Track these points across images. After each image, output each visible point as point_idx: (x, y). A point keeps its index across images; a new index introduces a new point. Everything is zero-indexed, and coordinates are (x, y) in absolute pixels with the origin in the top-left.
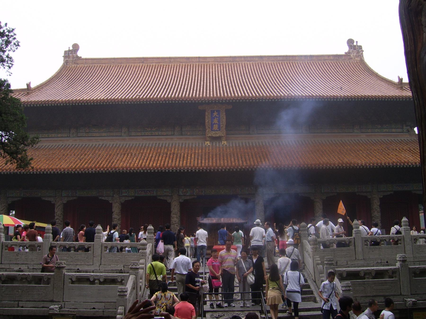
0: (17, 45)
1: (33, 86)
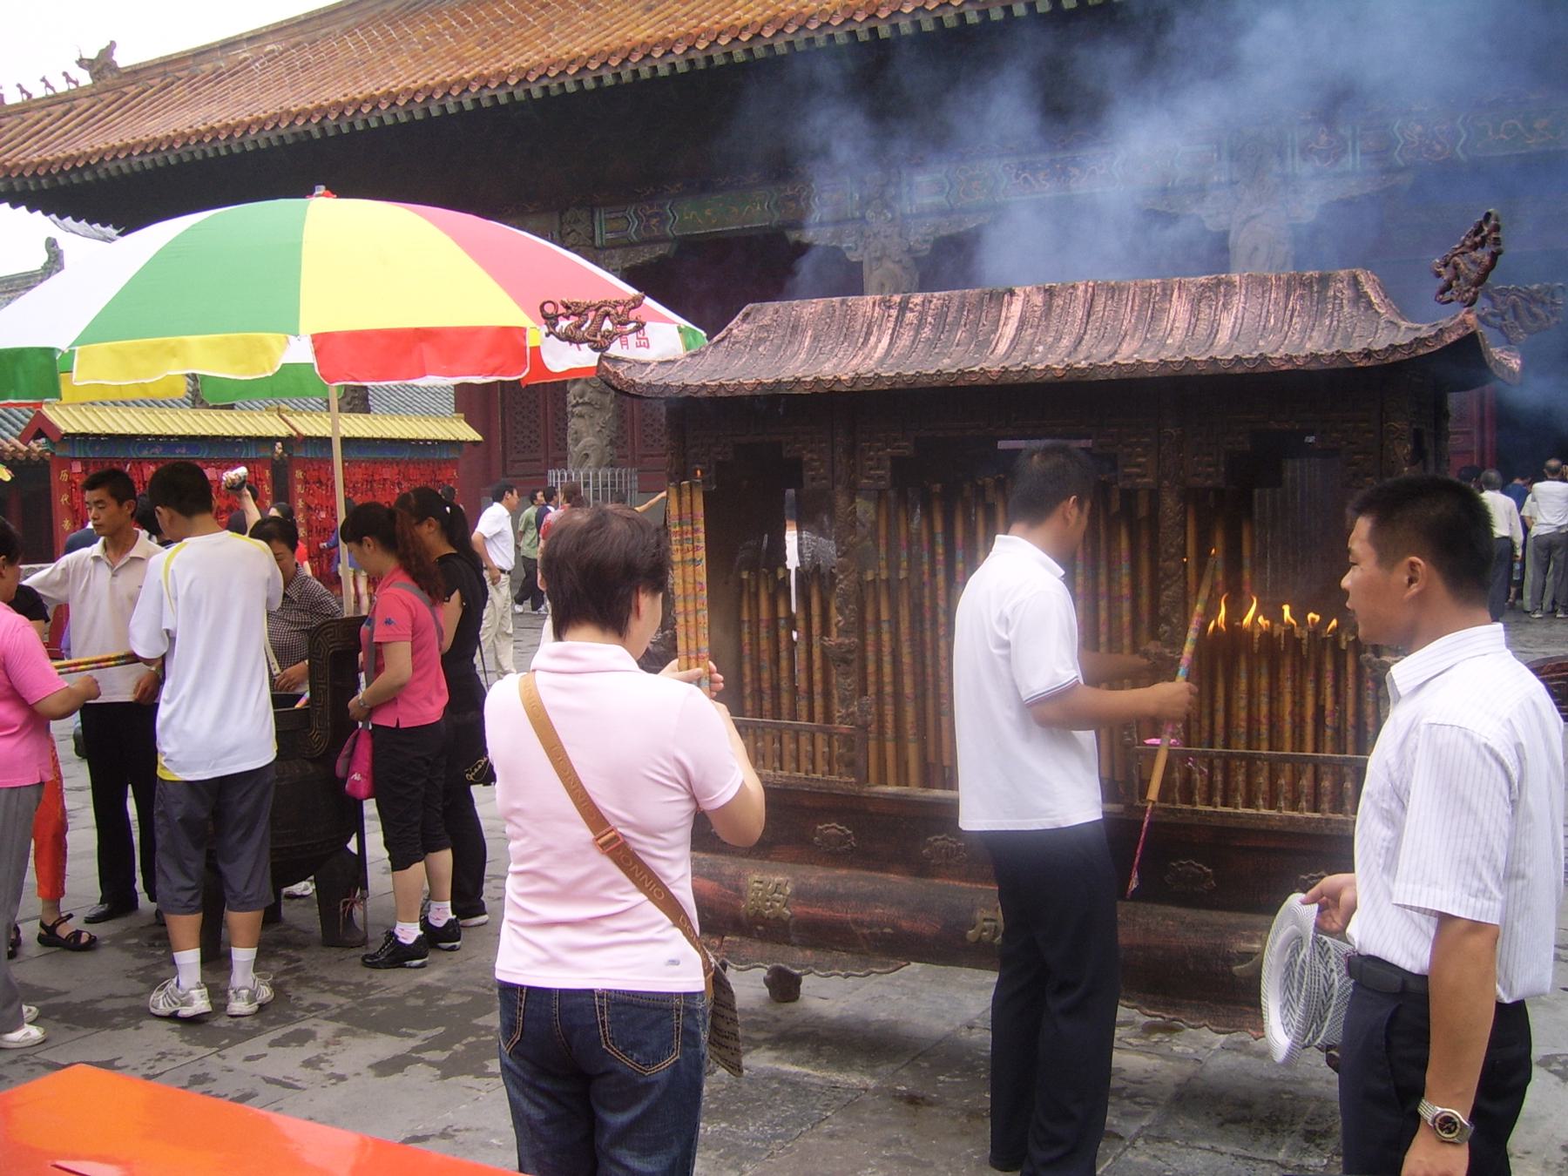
1: (123, 59)
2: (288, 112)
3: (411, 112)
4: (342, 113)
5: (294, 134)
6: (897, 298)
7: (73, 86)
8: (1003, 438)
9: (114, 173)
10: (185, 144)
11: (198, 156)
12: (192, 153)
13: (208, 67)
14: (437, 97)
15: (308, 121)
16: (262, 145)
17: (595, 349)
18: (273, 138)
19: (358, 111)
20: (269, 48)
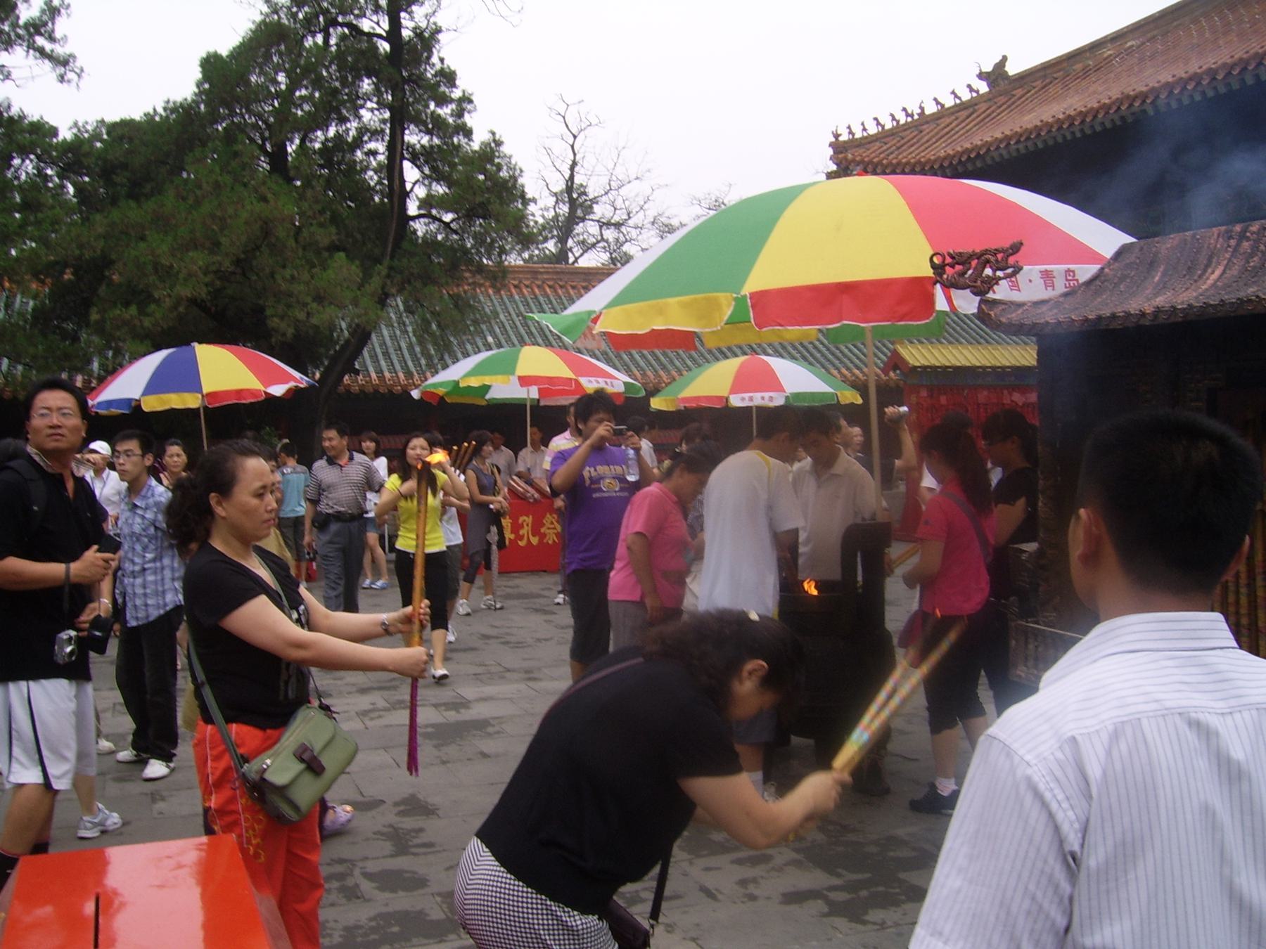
0: (168, 102)
1: (1012, 69)
2: (1128, 97)
3: (1229, 84)
4: (1171, 92)
5: (1133, 114)
6: (1238, 228)
7: (974, 95)
8: (1019, 371)
9: (998, 159)
10: (1050, 131)
11: (1060, 140)
12: (1054, 138)
13: (1078, 67)
14: (1250, 68)
15: (1144, 101)
16: (1108, 125)
17: (975, 294)
18: (1116, 118)
19: (1184, 88)
20: (1129, 44)
